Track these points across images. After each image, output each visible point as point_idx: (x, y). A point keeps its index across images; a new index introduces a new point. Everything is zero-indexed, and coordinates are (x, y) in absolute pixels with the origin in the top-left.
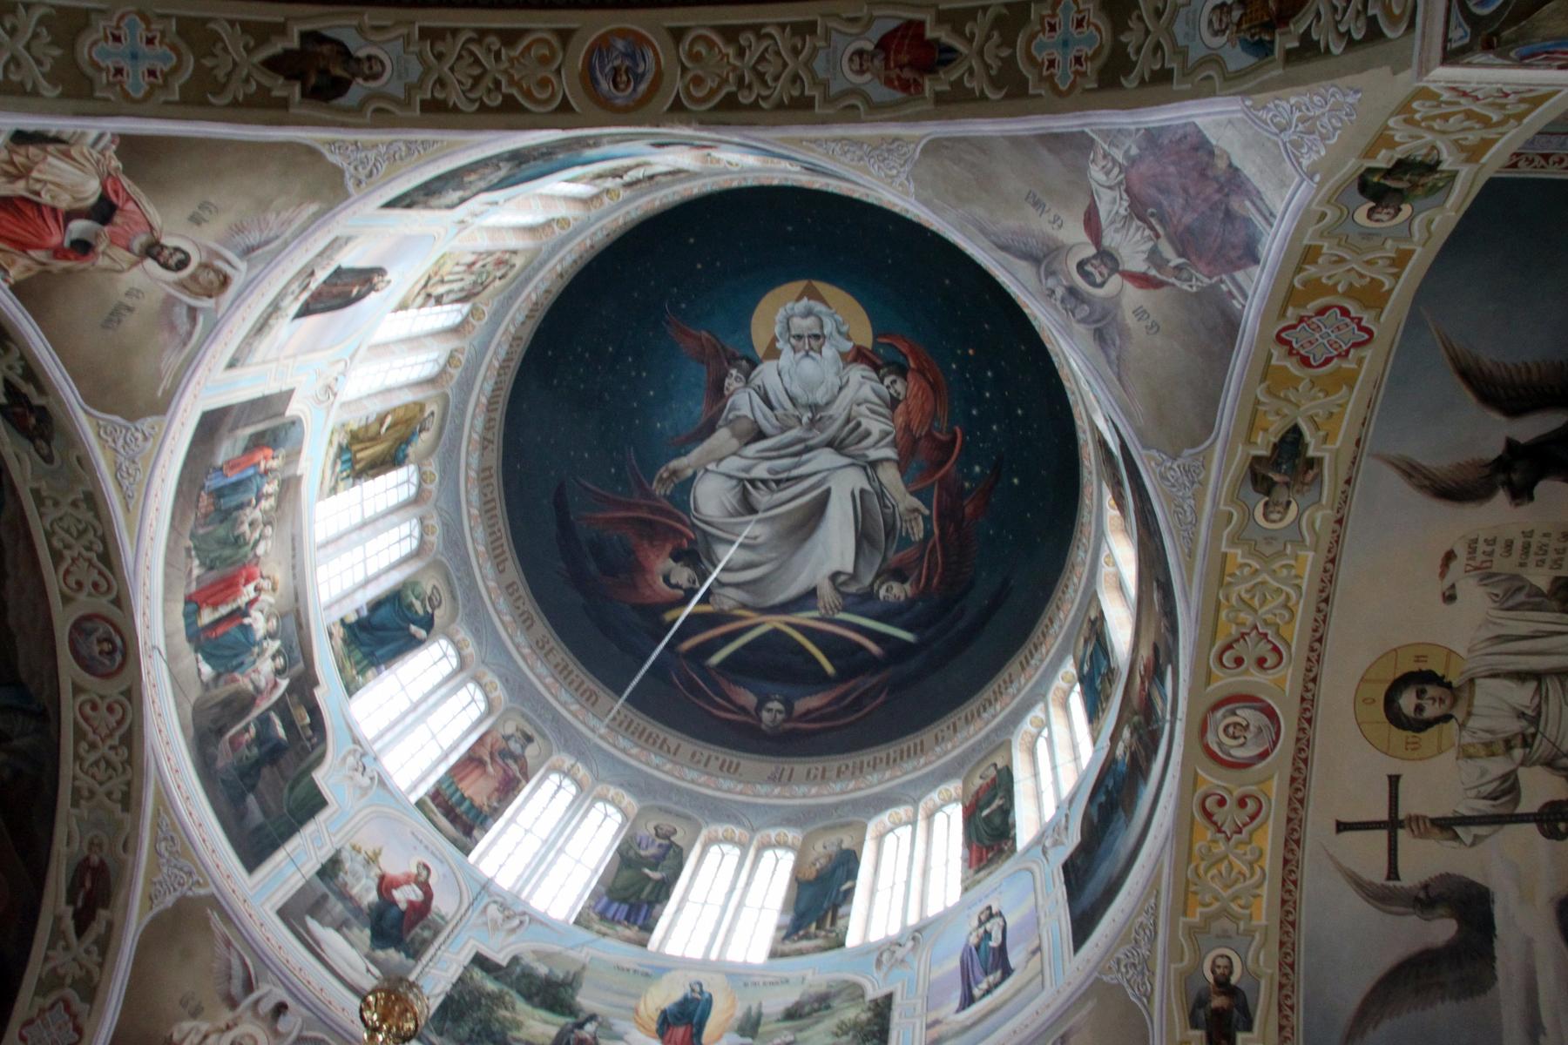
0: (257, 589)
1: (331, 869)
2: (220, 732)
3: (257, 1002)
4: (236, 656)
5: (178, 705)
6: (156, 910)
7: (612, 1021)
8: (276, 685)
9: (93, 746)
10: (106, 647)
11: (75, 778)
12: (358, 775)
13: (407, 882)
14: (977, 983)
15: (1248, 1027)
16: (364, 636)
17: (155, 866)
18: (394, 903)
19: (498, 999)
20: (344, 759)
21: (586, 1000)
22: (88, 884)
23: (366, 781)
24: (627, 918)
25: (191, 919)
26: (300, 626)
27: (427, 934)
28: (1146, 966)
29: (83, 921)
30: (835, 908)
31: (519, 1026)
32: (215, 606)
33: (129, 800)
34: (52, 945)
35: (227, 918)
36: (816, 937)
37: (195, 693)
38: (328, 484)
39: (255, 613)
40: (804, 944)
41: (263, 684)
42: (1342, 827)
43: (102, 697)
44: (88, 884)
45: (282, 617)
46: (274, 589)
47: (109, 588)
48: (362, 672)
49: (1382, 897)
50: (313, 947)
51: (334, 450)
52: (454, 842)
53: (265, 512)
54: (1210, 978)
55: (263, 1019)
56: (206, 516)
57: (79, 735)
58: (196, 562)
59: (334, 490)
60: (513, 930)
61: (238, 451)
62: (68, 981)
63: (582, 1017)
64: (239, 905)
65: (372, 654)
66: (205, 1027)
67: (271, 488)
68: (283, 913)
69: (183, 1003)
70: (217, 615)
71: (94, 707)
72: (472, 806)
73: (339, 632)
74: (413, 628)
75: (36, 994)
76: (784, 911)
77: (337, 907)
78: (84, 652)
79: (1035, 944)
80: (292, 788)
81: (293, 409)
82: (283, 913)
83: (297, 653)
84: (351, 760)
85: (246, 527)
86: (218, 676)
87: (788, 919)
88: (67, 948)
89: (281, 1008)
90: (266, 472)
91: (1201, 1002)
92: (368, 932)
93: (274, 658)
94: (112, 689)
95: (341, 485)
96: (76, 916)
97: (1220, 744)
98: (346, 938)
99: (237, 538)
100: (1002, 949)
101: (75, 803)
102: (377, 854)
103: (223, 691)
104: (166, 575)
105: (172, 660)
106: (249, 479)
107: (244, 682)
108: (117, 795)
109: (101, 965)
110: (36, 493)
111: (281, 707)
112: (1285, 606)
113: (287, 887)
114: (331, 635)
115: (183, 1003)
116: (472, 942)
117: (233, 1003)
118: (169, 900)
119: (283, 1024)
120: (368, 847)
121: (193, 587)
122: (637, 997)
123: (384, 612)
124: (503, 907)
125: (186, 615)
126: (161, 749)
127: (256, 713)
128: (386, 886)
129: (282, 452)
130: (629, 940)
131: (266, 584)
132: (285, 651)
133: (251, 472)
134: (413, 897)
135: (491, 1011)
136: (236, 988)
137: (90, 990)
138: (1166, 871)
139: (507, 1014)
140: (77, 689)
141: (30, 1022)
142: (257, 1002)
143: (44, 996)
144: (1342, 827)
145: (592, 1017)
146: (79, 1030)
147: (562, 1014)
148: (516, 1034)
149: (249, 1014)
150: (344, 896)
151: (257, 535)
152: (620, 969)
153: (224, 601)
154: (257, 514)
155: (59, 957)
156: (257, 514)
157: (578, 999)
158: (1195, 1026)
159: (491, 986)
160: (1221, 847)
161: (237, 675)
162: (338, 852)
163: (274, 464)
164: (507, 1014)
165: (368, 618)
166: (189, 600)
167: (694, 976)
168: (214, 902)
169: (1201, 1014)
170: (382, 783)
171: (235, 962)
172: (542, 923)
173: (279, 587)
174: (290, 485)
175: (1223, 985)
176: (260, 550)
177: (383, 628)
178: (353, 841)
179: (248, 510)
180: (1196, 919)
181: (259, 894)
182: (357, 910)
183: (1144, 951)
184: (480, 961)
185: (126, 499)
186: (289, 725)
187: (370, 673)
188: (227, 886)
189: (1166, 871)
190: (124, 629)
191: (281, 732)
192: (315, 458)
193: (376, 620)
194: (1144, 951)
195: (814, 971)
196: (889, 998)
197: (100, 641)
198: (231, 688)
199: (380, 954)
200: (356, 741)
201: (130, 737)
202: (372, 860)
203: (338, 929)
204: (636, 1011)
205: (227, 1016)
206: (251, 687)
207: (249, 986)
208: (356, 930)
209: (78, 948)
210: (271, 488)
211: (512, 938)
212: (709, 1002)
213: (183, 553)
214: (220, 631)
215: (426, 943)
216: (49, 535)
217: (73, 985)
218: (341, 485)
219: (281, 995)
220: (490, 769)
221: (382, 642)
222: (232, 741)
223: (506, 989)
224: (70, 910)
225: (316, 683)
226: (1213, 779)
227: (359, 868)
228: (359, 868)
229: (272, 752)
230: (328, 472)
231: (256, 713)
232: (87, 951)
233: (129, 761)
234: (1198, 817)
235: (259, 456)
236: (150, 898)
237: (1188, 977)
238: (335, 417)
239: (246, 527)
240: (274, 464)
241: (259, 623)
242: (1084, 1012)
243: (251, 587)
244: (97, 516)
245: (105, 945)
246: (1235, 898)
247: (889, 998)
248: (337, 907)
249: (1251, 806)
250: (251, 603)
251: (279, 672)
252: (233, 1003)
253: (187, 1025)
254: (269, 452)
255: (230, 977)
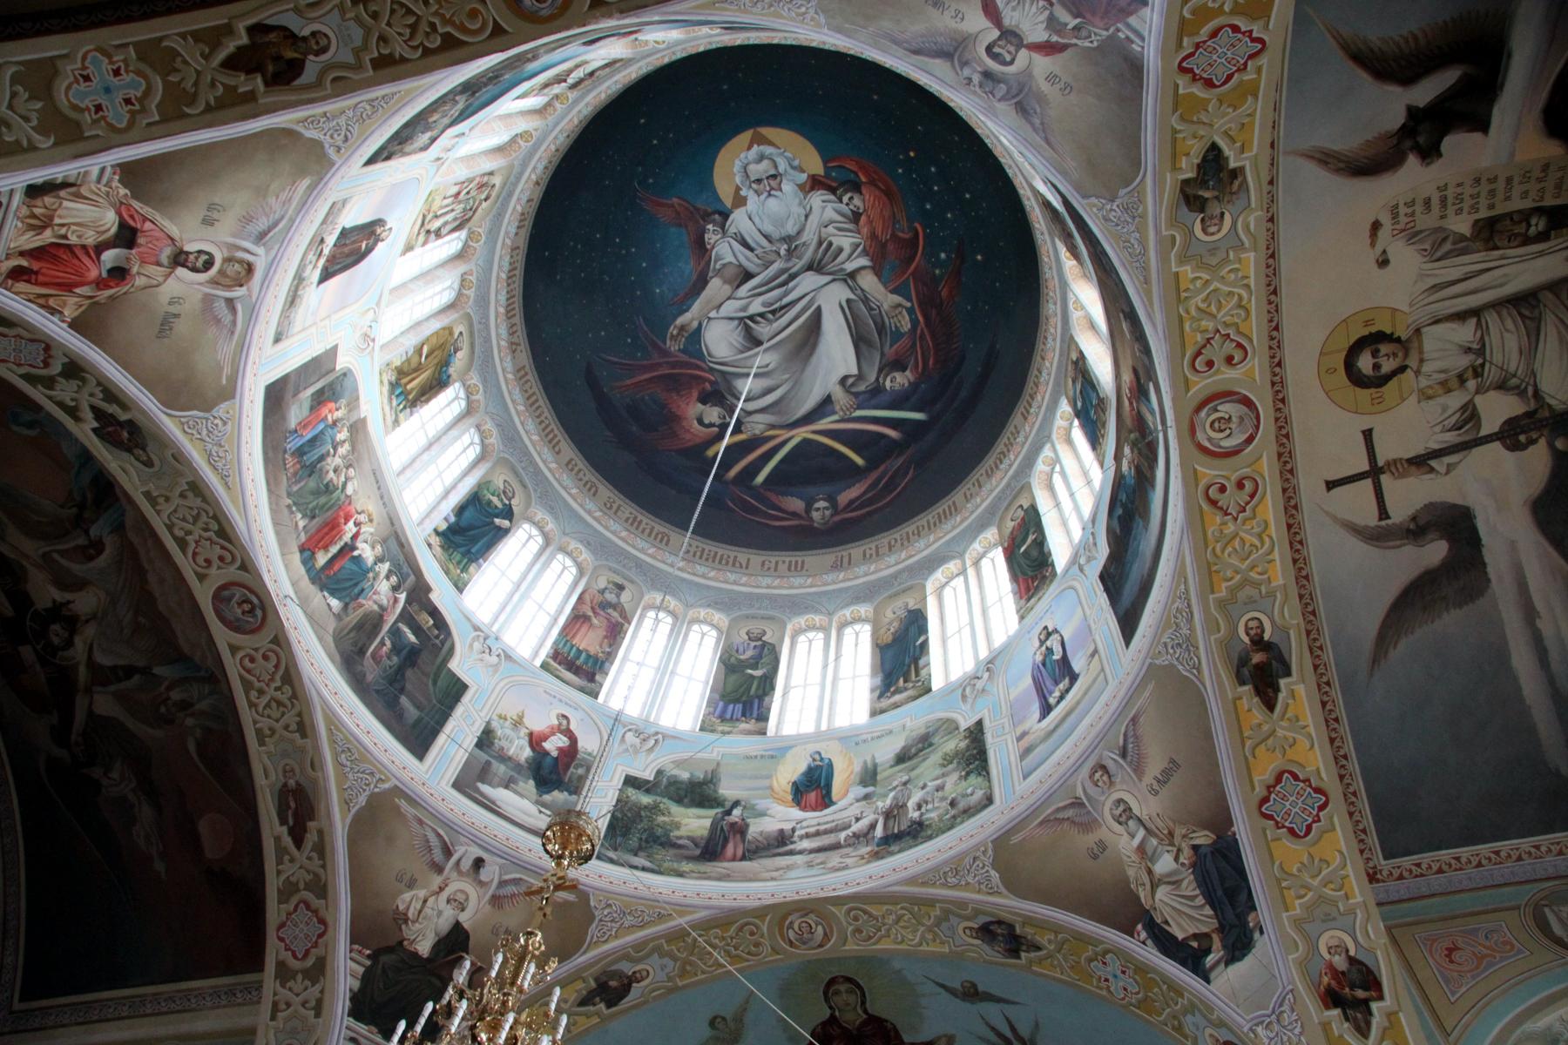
0: (356, 524)
1: (486, 740)
2: (362, 652)
3: (458, 863)
4: (356, 585)
5: (320, 639)
6: (353, 811)
7: (754, 802)
8: (396, 600)
9: (261, 692)
10: (246, 607)
11: (255, 722)
12: (486, 656)
13: (553, 734)
14: (1051, 693)
15: (1288, 674)
16: (458, 539)
17: (342, 777)
18: (547, 753)
19: (654, 809)
20: (471, 646)
21: (727, 791)
22: (293, 804)
23: (494, 659)
24: (744, 715)
25: (384, 810)
26: (402, 546)
27: (581, 771)
28: (1190, 644)
29: (298, 837)
30: (916, 660)
31: (678, 826)
32: (326, 548)
33: (304, 727)
34: (279, 862)
35: (412, 801)
36: (906, 689)
37: (332, 625)
38: (390, 419)
39: (360, 545)
40: (897, 698)
41: (385, 602)
42: (1331, 485)
43: (256, 650)
44: (293, 804)
45: (384, 541)
46: (371, 521)
47: (234, 559)
48: (465, 569)
49: (1377, 537)
50: (491, 807)
51: (386, 388)
52: (582, 690)
53: (344, 457)
54: (1246, 640)
55: (467, 874)
56: (295, 474)
57: (247, 686)
58: (299, 516)
59: (396, 422)
60: (651, 749)
61: (306, 411)
62: (302, 886)
63: (728, 805)
64: (422, 790)
65: (469, 552)
66: (422, 893)
67: (342, 435)
68: (457, 785)
69: (399, 879)
70: (330, 555)
71: (252, 660)
72: (589, 656)
73: (436, 541)
74: (497, 521)
75: (280, 902)
76: (874, 674)
77: (500, 769)
78: (228, 615)
79: (1092, 648)
80: (435, 683)
81: (342, 363)
82: (457, 785)
83: (406, 569)
84: (477, 645)
85: (331, 474)
86: (346, 606)
87: (878, 680)
88: (292, 860)
89: (479, 863)
90: (335, 423)
91: (1243, 661)
92: (532, 782)
93: (387, 577)
94: (262, 640)
95: (401, 416)
96: (291, 832)
97: (1210, 439)
98: (516, 792)
99: (327, 486)
100: (1065, 660)
101: (262, 743)
102: (521, 717)
103: (353, 617)
104: (277, 533)
105: (304, 603)
106: (322, 432)
107: (369, 604)
108: (294, 727)
109: (324, 867)
110: (147, 494)
111: (405, 617)
112: (1240, 306)
113: (451, 770)
114: (430, 545)
115: (399, 879)
116: (620, 768)
117: (439, 869)
118: (362, 800)
119: (485, 874)
120: (512, 714)
121: (303, 538)
122: (769, 777)
123: (468, 514)
124: (638, 733)
125: (304, 562)
126: (318, 679)
127: (386, 627)
128: (535, 741)
129: (343, 402)
130: (749, 733)
131: (362, 518)
132: (395, 570)
133: (321, 426)
134: (561, 744)
135: (651, 820)
136: (438, 855)
137: (321, 888)
138: (1188, 560)
139: (666, 819)
140: (234, 649)
141: (282, 925)
142: (458, 863)
143: (287, 901)
144: (1331, 485)
145: (736, 804)
146: (322, 921)
147: (711, 807)
148: (677, 833)
149: (454, 875)
150: (504, 758)
151: (343, 479)
152: (748, 758)
153: (332, 543)
154: (338, 461)
155: (289, 869)
156: (338, 461)
157: (721, 791)
158: (1242, 683)
159: (646, 800)
160: (1231, 528)
161: (361, 600)
162: (488, 723)
163: (338, 414)
164: (666, 819)
165: (457, 523)
166: (302, 549)
167: (812, 748)
168: (398, 791)
169: (1245, 671)
170: (508, 657)
171: (434, 841)
172: (674, 737)
173: (374, 517)
174: (358, 429)
175: (1259, 642)
176: (349, 490)
177: (471, 528)
178: (499, 711)
179: (329, 460)
180: (1223, 593)
181: (433, 775)
182: (518, 767)
183: (1185, 631)
184: (630, 781)
185: (224, 478)
186: (417, 630)
187: (472, 568)
188: (405, 776)
189: (1188, 560)
190: (251, 584)
191: (412, 638)
192: (372, 399)
193: (463, 523)
194: (1185, 631)
195: (912, 718)
196: (980, 723)
197: (240, 604)
198: (361, 611)
199: (547, 798)
200: (477, 629)
201: (289, 676)
202: (518, 723)
203: (506, 787)
204: (771, 788)
205: (437, 880)
206: (376, 607)
207: (448, 853)
208: (521, 784)
209: (301, 857)
210: (342, 435)
211: (652, 756)
212: (830, 765)
213: (286, 511)
214: (336, 568)
215: (582, 779)
216: (170, 528)
217: (308, 887)
218: (401, 416)
219: (477, 852)
220: (595, 621)
221: (474, 540)
222: (373, 656)
223: (659, 799)
224: (284, 829)
225: (429, 589)
226: (1210, 472)
227: (508, 732)
228: (508, 732)
229: (410, 657)
230: (387, 408)
231: (386, 627)
232: (309, 858)
233: (294, 696)
234: (1205, 506)
235: (325, 411)
236: (347, 803)
237: (1226, 645)
238: (379, 359)
239: (331, 474)
240: (338, 414)
241: (366, 552)
242: (1146, 694)
243: (351, 524)
244: (205, 500)
245: (322, 849)
246: (1252, 568)
247: (980, 723)
248: (500, 769)
249: (1248, 486)
250: (355, 537)
251: (395, 589)
252: (439, 869)
253: (407, 896)
254: (332, 405)
255: (430, 850)
